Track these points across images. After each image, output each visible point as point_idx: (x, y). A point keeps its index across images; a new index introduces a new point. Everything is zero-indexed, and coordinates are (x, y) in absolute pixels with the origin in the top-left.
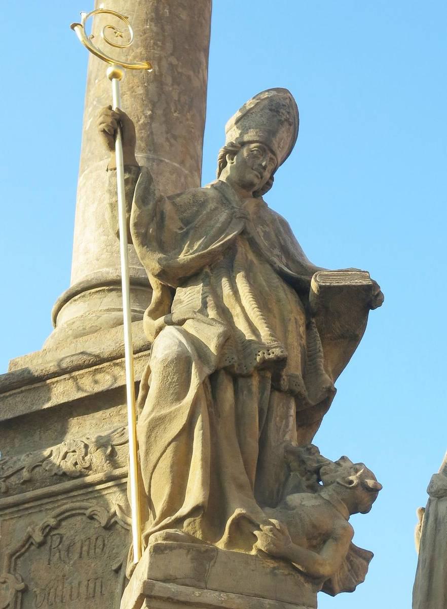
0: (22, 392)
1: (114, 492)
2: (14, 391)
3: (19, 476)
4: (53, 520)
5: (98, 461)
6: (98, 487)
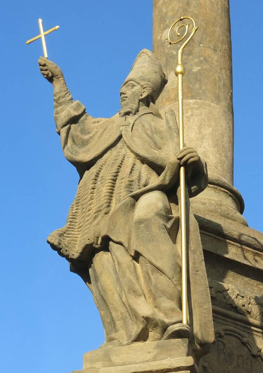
0: (210, 236)
1: (260, 336)
2: (206, 233)
5: (255, 312)
6: (253, 328)
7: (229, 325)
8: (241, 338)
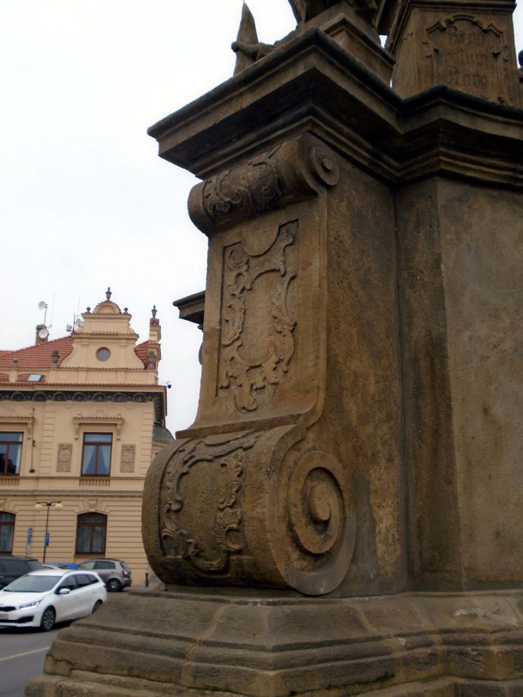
8: (471, 19)
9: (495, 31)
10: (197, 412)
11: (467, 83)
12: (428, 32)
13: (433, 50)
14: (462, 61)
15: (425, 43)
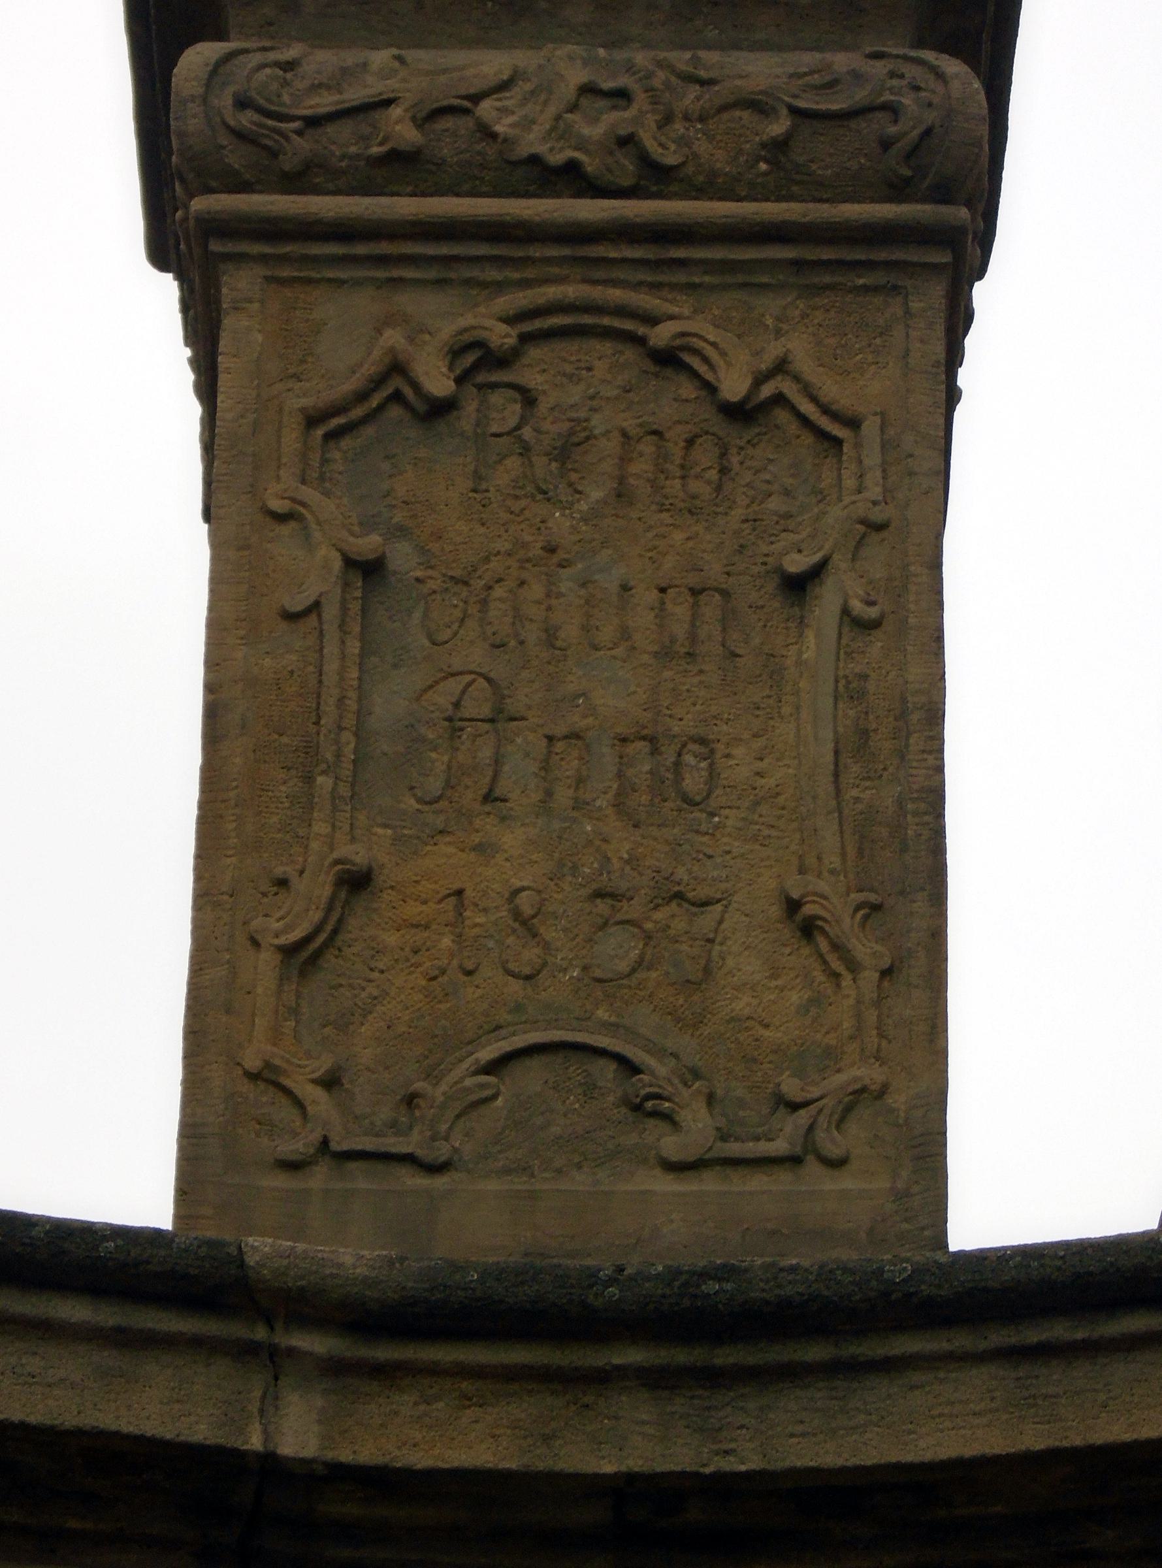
3: (366, 130)
4: (503, 328)
7: (547, 281)
8: (641, 330)
9: (807, 408)
10: (1030, 1242)
11: (563, 796)
12: (320, 432)
13: (337, 564)
14: (550, 636)
15: (281, 518)
